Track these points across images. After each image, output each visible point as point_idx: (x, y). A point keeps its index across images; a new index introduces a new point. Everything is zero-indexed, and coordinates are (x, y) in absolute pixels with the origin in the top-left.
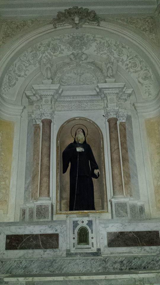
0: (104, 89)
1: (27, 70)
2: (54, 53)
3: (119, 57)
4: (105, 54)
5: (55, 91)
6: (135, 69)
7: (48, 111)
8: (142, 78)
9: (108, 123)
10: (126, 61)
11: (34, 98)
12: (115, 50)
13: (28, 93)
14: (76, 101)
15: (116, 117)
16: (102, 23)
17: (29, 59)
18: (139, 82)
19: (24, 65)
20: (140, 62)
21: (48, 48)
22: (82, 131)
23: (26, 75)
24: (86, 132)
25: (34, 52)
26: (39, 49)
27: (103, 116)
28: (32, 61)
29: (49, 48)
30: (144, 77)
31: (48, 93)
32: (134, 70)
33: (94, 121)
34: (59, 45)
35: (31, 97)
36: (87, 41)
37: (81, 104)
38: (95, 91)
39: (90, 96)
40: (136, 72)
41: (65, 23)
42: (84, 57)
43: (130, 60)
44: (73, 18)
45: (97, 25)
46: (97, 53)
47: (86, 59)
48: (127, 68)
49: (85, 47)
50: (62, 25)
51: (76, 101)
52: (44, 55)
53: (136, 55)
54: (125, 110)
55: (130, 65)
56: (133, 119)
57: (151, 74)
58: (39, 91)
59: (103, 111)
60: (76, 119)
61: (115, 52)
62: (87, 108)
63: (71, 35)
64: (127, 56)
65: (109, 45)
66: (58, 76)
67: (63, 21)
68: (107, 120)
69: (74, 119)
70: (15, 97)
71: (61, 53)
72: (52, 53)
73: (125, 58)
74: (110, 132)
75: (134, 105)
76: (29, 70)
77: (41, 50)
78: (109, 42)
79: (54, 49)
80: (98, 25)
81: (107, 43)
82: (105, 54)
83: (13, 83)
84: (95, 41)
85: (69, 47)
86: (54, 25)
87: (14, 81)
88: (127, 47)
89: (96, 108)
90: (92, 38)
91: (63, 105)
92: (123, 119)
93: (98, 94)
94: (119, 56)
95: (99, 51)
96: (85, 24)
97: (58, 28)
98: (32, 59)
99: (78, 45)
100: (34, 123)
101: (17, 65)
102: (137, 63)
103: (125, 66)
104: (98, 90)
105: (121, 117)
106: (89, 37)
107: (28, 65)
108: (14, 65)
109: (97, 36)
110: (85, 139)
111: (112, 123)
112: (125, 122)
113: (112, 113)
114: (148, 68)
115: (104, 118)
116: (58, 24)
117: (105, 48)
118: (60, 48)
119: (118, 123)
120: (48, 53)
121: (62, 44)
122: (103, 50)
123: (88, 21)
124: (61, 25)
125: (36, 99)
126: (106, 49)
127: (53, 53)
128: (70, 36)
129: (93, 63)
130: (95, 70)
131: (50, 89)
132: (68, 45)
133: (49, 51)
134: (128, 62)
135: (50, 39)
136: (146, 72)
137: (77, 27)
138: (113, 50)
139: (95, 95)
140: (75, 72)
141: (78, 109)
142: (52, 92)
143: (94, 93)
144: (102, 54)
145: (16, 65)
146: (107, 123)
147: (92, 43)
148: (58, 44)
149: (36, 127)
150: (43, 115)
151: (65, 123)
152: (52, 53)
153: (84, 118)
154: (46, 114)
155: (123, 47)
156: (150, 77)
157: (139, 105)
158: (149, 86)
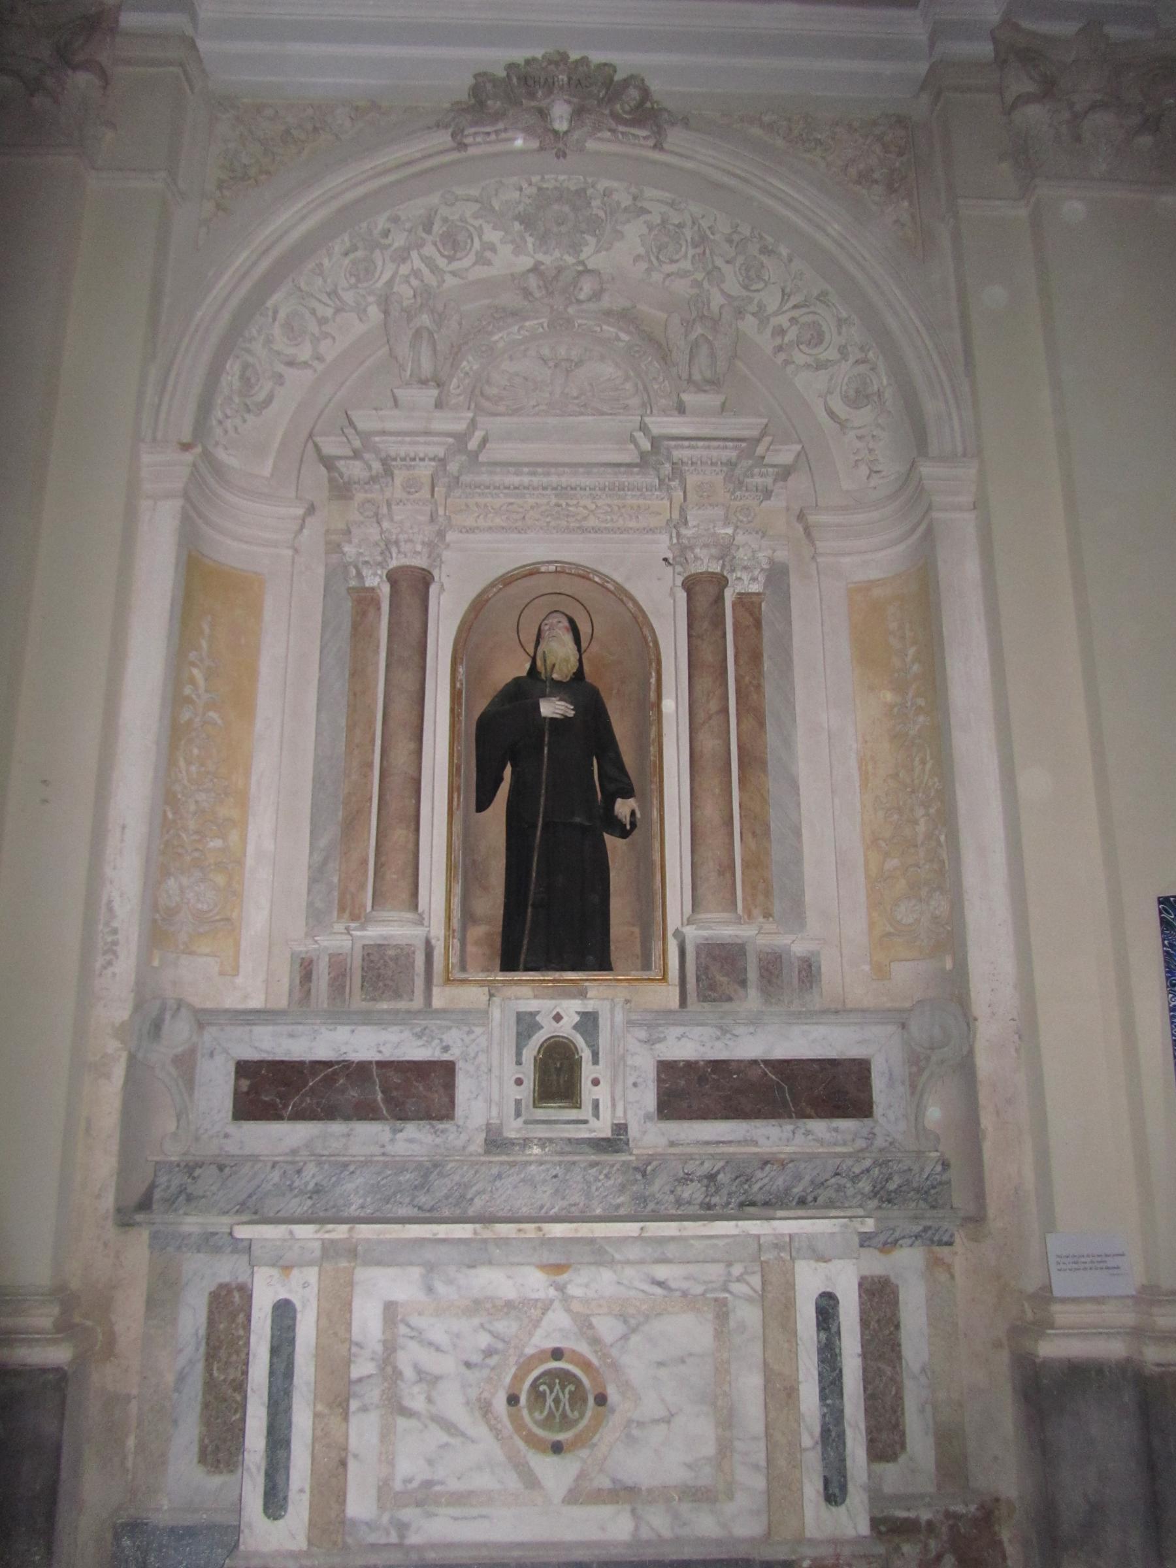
0: (673, 443)
1: (326, 335)
2: (451, 259)
3: (745, 293)
4: (683, 274)
5: (451, 440)
6: (814, 351)
7: (416, 530)
8: (845, 398)
9: (685, 594)
10: (776, 314)
11: (355, 470)
12: (728, 262)
13: (331, 446)
14: (545, 488)
15: (718, 570)
16: (675, 137)
17: (336, 286)
18: (831, 414)
19: (313, 312)
20: (841, 322)
21: (424, 235)
22: (566, 623)
23: (320, 358)
24: (584, 628)
25: (360, 254)
26: (383, 241)
27: (665, 560)
28: (349, 297)
29: (429, 238)
30: (852, 393)
31: (421, 450)
32: (810, 360)
33: (619, 580)
34: (477, 223)
35: (341, 464)
36: (602, 214)
37: (567, 504)
38: (632, 446)
39: (609, 470)
40: (820, 366)
41: (506, 130)
42: (587, 286)
43: (796, 313)
44: (544, 104)
45: (651, 143)
46: (649, 271)
47: (597, 295)
48: (780, 349)
49: (592, 240)
50: (493, 137)
51: (545, 488)
52: (404, 269)
53: (824, 293)
54: (763, 537)
55: (791, 335)
56: (794, 580)
57: (885, 382)
58: (377, 439)
59: (665, 537)
60: (543, 569)
61: (727, 269)
62: (592, 522)
63: (530, 184)
64: (783, 291)
65: (703, 239)
66: (467, 368)
67: (497, 116)
68: (679, 580)
69: (532, 572)
70: (270, 463)
71: (481, 260)
72: (442, 262)
73: (772, 302)
74: (689, 636)
75: (801, 517)
76: (334, 338)
77: (390, 245)
78: (704, 224)
79: (453, 242)
80: (658, 147)
81: (696, 228)
82: (683, 274)
83: (262, 396)
84: (639, 216)
85: (523, 239)
86: (453, 135)
87: (268, 385)
88: (784, 251)
89: (632, 524)
90: (626, 201)
91: (486, 506)
92: (754, 579)
93: (644, 462)
94: (746, 288)
95: (658, 258)
96: (599, 135)
97: (472, 151)
98: (351, 287)
99: (563, 229)
100: (353, 583)
101: (282, 315)
102: (825, 328)
103: (773, 335)
104: (646, 445)
105: (745, 568)
106: (615, 196)
107: (329, 312)
108: (270, 313)
109: (650, 192)
110: (580, 661)
111: (703, 594)
112: (758, 594)
113: (705, 551)
114: (871, 355)
115: (670, 569)
116: (473, 130)
117: (683, 249)
118: (480, 238)
119: (729, 596)
120: (423, 259)
121: (488, 222)
122: (677, 257)
123: (613, 124)
124: (488, 134)
125: (365, 475)
126: (691, 252)
127: (446, 261)
128: (525, 186)
129: (626, 317)
130: (637, 349)
131: (427, 433)
132: (517, 226)
133: (429, 250)
134: (783, 320)
135: (435, 199)
136: (862, 368)
137: (561, 145)
138: (719, 262)
139: (629, 465)
140: (546, 351)
141: (553, 524)
142: (439, 444)
143: (629, 455)
144: (668, 275)
145: (276, 312)
146: (682, 595)
147: (628, 221)
148: (471, 221)
149: (359, 602)
150: (394, 550)
151: (492, 585)
152: (442, 262)
153: (578, 566)
154: (409, 546)
155: (765, 250)
156: (879, 394)
157: (823, 518)
158: (873, 436)
